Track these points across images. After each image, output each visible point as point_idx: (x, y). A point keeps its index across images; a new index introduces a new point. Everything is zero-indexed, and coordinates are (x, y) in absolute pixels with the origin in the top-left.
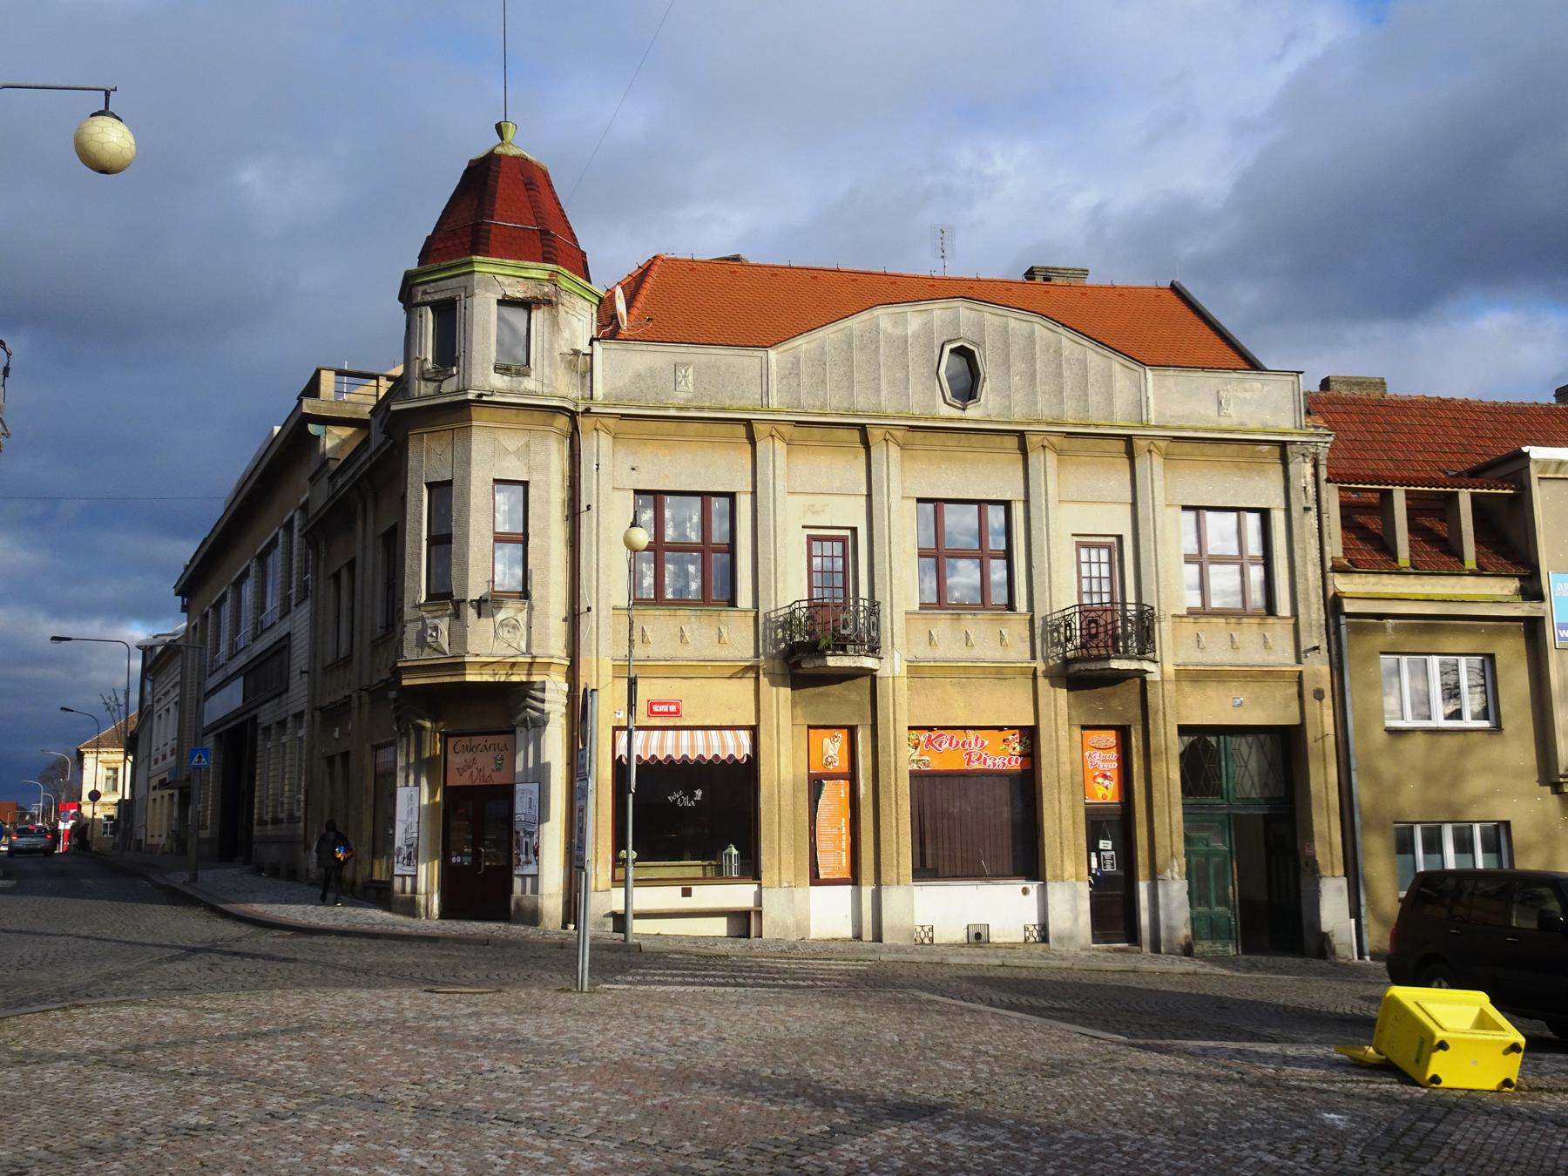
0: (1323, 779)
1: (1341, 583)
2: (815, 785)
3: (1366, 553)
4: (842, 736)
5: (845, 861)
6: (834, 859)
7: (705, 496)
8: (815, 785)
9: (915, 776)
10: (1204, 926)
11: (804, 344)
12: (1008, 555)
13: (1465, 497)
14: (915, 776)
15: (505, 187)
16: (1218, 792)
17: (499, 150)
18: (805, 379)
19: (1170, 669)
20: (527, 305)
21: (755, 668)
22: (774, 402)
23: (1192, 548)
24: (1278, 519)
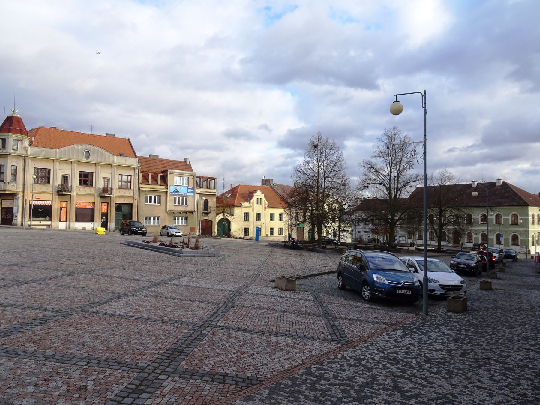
0: (135, 210)
1: (141, 186)
2: (61, 209)
3: (146, 182)
4: (66, 202)
5: (65, 219)
6: (63, 218)
7: (128, 176)
8: (61, 209)
9: (76, 208)
10: (116, 229)
11: (63, 149)
12: (131, 182)
13: (159, 176)
14: (76, 208)
15: (14, 122)
16: (121, 212)
17: (13, 115)
18: (63, 154)
19: (115, 196)
20: (18, 140)
21: (52, 193)
22: (57, 157)
23: (120, 180)
24: (133, 177)
